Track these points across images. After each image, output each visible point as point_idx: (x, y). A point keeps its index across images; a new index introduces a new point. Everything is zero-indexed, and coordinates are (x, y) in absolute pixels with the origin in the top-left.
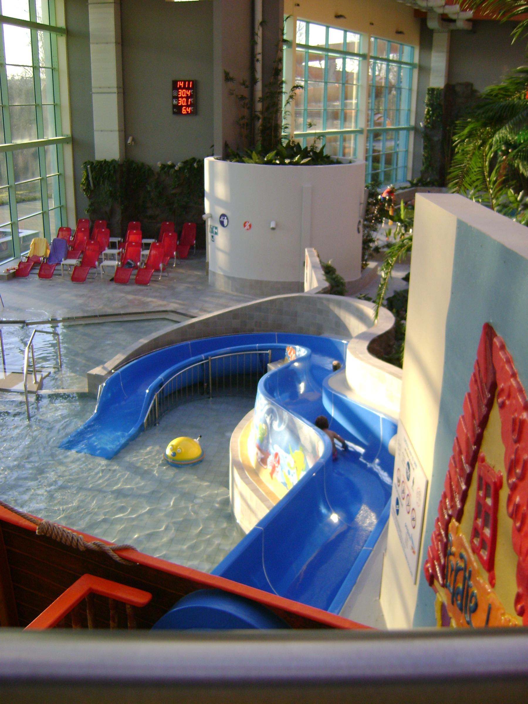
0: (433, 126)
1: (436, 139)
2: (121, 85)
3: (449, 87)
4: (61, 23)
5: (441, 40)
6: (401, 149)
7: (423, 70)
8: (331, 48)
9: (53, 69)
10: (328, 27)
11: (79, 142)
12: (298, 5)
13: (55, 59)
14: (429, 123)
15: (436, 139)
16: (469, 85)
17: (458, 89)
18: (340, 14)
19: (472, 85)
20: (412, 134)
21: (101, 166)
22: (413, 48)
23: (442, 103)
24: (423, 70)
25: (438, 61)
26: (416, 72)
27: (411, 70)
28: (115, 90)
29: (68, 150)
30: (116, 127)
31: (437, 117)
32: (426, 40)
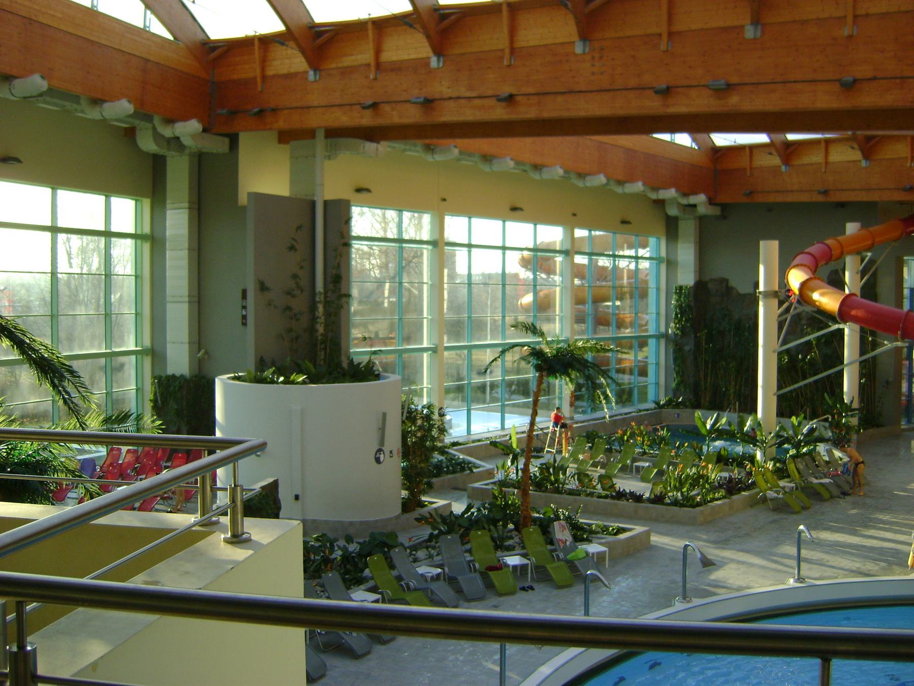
0: (682, 331)
1: (687, 348)
2: (196, 293)
3: (700, 286)
4: (147, 230)
5: (688, 228)
6: (652, 360)
7: (671, 264)
8: (540, 247)
9: (136, 277)
10: (470, 218)
11: (155, 353)
12: (445, 200)
13: (139, 266)
14: (678, 329)
15: (687, 348)
16: (724, 281)
17: (710, 286)
18: (518, 205)
19: (727, 281)
20: (663, 342)
21: (168, 380)
22: (659, 239)
23: (692, 304)
24: (671, 264)
25: (686, 254)
26: (663, 267)
27: (658, 265)
28: (187, 299)
29: (148, 361)
30: (186, 338)
31: (686, 321)
32: (671, 229)
